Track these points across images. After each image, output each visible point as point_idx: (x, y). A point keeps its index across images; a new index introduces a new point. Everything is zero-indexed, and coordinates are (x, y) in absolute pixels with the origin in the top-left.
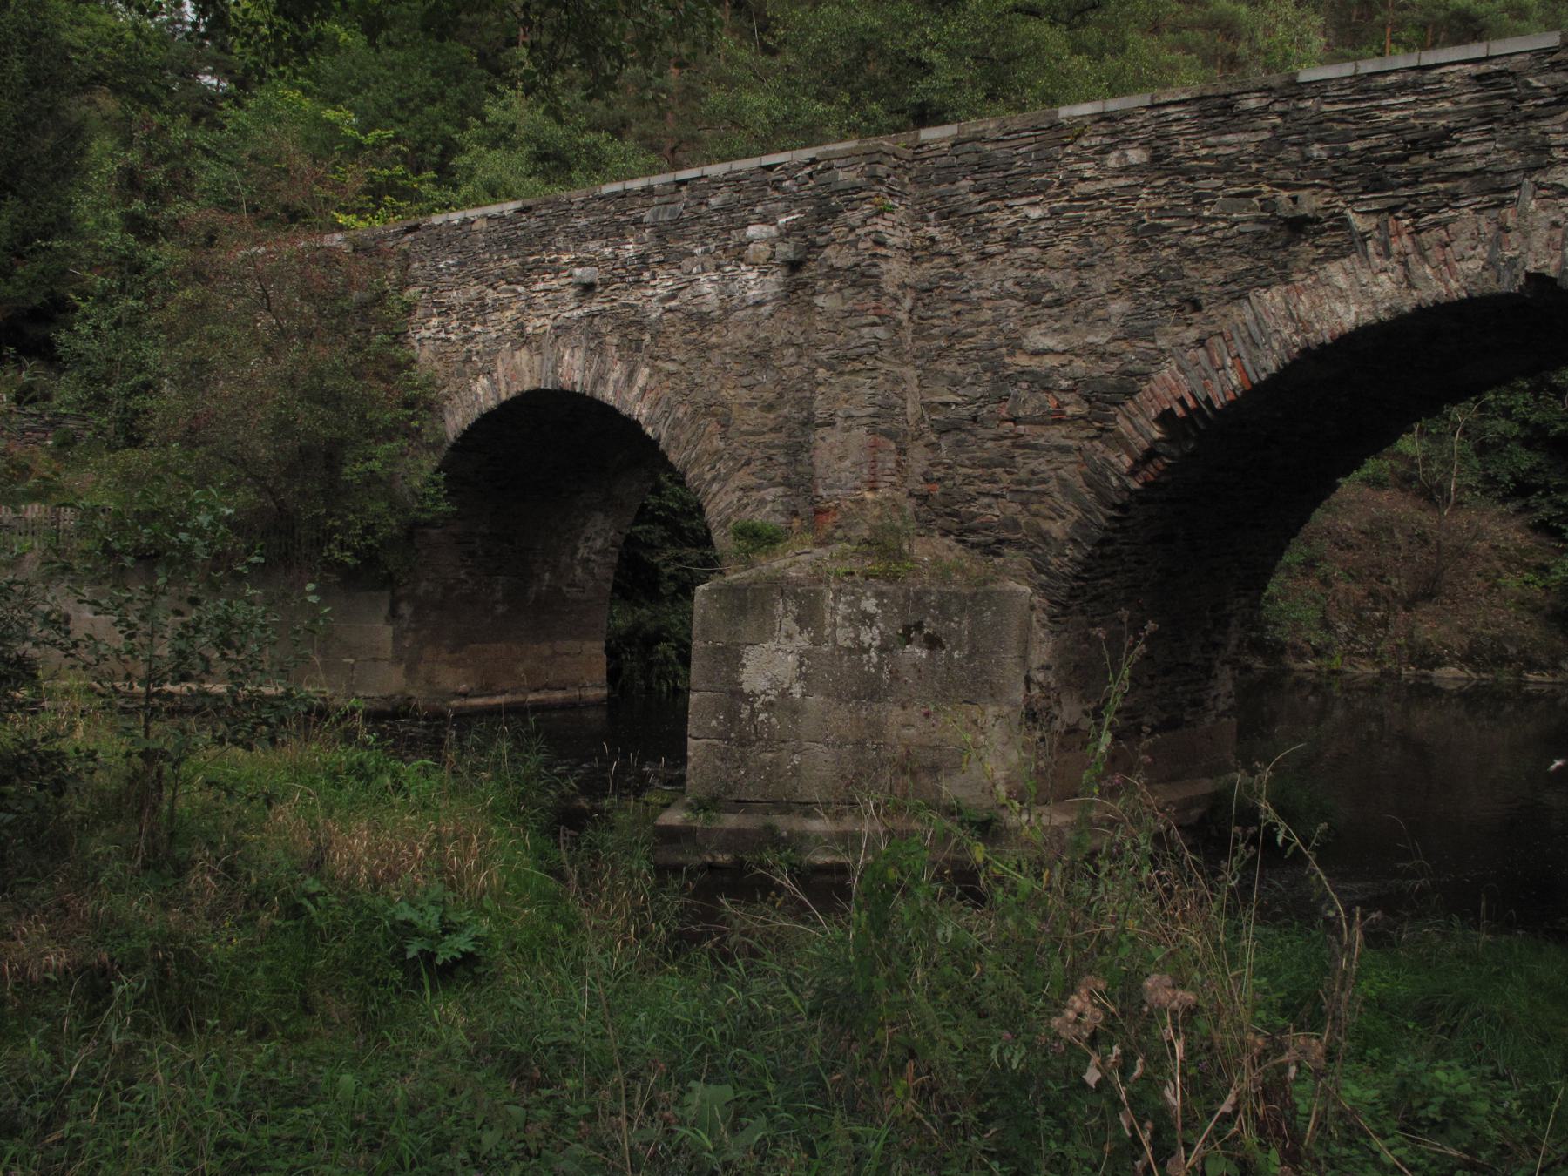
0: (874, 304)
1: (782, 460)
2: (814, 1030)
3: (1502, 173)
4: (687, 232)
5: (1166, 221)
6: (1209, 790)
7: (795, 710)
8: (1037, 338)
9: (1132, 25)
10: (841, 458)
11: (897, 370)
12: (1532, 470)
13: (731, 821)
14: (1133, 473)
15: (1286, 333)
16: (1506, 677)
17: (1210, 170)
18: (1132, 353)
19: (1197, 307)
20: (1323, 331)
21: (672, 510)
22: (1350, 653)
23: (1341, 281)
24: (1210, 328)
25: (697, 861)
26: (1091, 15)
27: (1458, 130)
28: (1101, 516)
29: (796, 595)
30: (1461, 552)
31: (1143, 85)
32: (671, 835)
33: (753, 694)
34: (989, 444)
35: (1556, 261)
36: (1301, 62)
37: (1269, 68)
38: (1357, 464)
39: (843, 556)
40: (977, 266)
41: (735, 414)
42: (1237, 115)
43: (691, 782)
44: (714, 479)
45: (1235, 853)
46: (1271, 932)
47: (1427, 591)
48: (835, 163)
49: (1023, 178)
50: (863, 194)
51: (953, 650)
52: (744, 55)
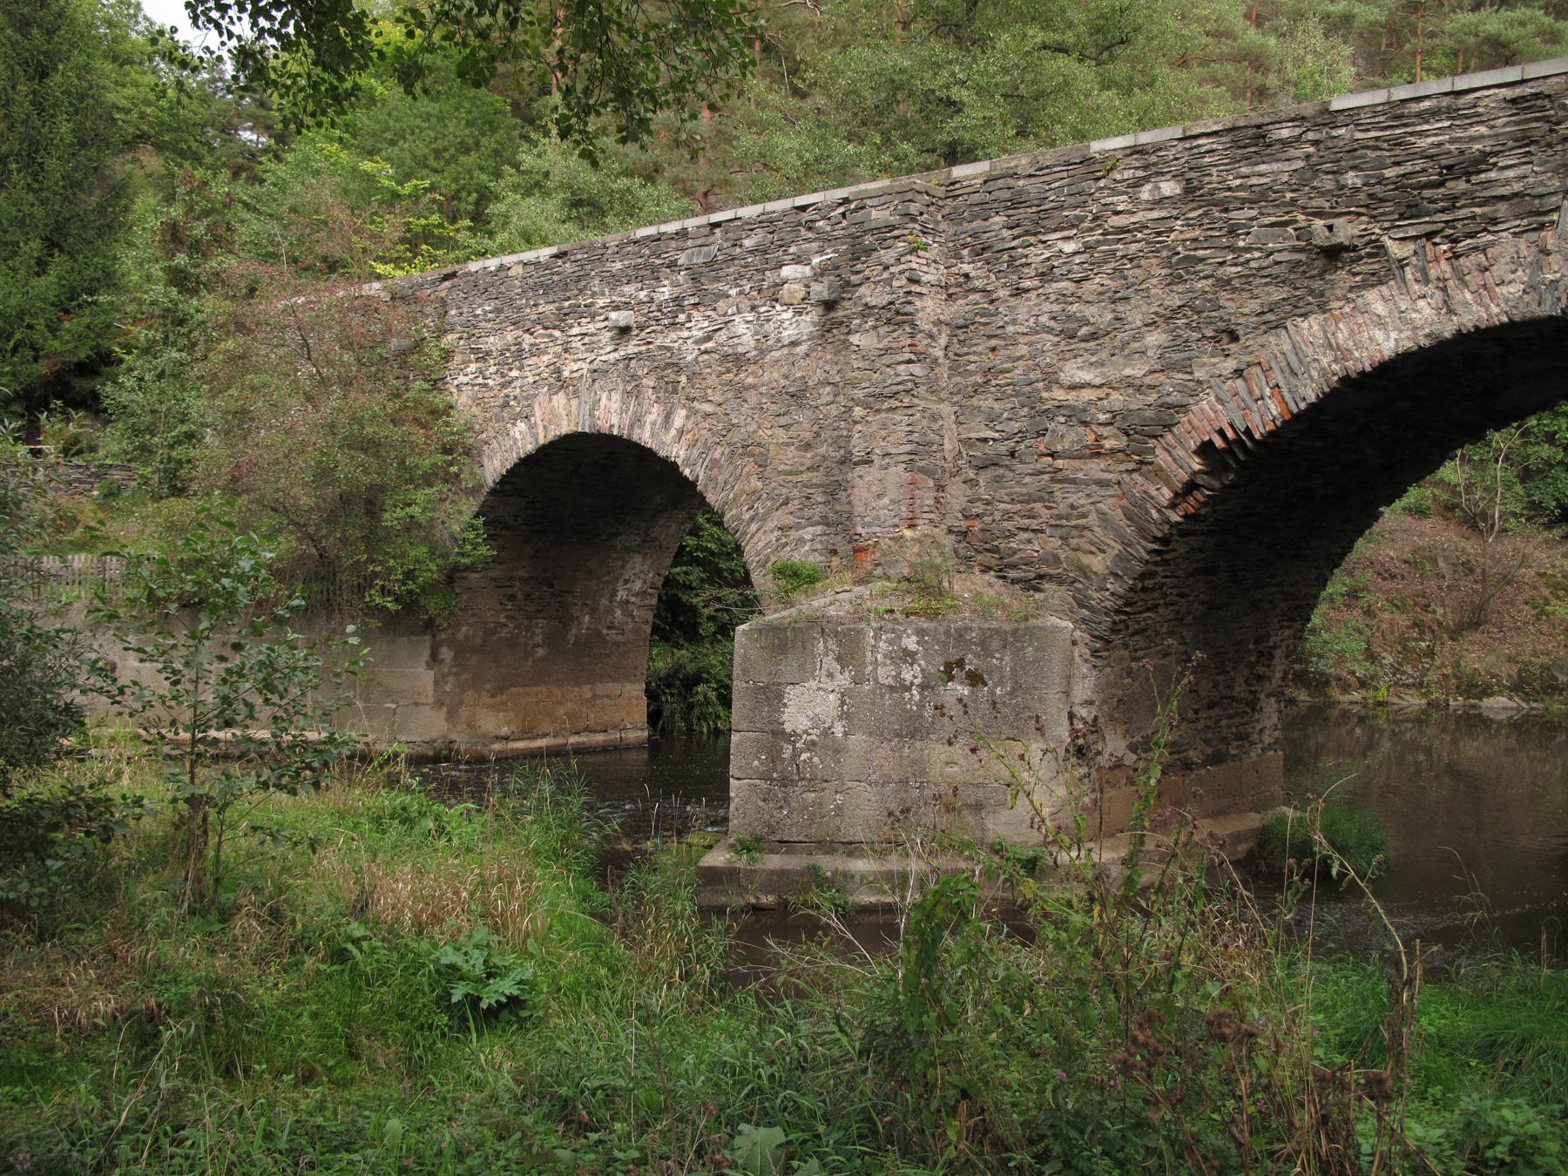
0: (909, 341)
2: (864, 1071)
3: (1541, 196)
4: (721, 273)
5: (1201, 253)
6: (1257, 824)
8: (1075, 372)
9: (1161, 60)
10: (879, 496)
13: (774, 862)
14: (1173, 506)
17: (1244, 201)
18: (1170, 385)
19: (1234, 338)
20: (1364, 359)
21: (712, 553)
23: (1380, 308)
25: (742, 903)
26: (1119, 50)
27: (1496, 154)
28: (1142, 549)
30: (1507, 580)
32: (713, 877)
34: (1028, 479)
36: (1331, 92)
38: (1400, 492)
39: (883, 595)
40: (1013, 302)
44: (752, 519)
47: (1473, 620)
48: (868, 202)
49: (1057, 213)
50: (896, 233)
51: (995, 686)
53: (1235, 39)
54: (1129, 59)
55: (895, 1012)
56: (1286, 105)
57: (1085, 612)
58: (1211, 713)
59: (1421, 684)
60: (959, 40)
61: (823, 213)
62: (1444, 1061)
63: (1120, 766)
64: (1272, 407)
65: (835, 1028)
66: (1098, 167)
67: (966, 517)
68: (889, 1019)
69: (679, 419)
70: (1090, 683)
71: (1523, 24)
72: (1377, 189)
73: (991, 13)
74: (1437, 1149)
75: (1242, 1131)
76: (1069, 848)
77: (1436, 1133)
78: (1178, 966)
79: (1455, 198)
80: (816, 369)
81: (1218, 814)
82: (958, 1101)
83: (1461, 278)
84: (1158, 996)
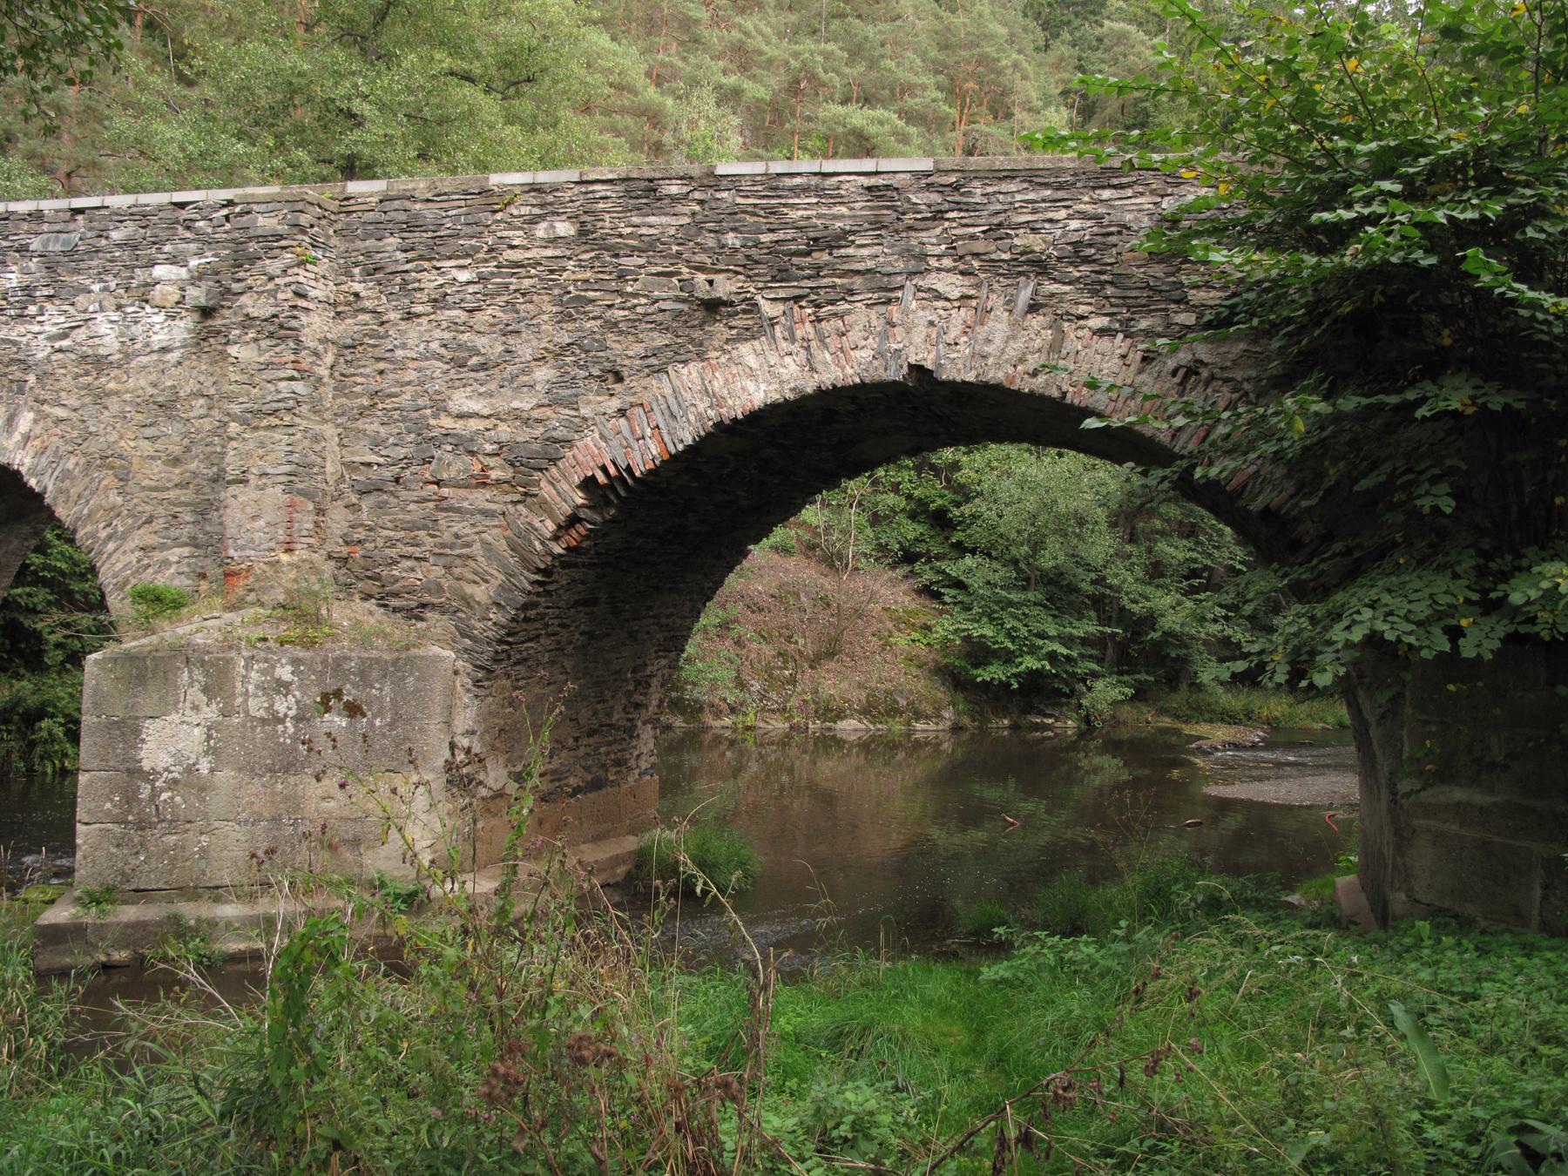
0: (293, 357)
1: (188, 519)
2: (226, 1135)
3: (889, 275)
4: (82, 265)
5: (591, 294)
6: (635, 847)
7: (203, 788)
8: (462, 400)
9: (566, 103)
10: (255, 518)
11: (317, 428)
12: (916, 540)
13: (130, 913)
14: (556, 538)
15: (701, 407)
16: (897, 726)
17: (634, 249)
18: (557, 420)
19: (619, 378)
20: (736, 407)
21: (62, 573)
22: (763, 709)
23: (752, 361)
24: (631, 399)
25: (89, 961)
26: (525, 88)
27: (853, 233)
28: (525, 580)
29: (203, 663)
30: (858, 614)
31: (573, 161)
32: (55, 935)
33: (154, 771)
34: (412, 507)
35: (932, 356)
36: (720, 157)
37: (691, 159)
38: (766, 532)
39: (256, 622)
40: (403, 325)
41: (135, 467)
42: (660, 199)
43: (80, 873)
44: (110, 537)
45: (656, 907)
46: (695, 980)
47: (829, 651)
48: (255, 207)
49: (452, 241)
50: (284, 243)
51: (375, 717)
52: (156, 81)
53: (636, 94)
54: (538, 100)
55: (261, 1066)
56: (679, 164)
57: (468, 641)
58: (591, 741)
59: (784, 710)
60: (364, 52)
61: (205, 213)
62: (799, 1056)
63: (501, 796)
64: (652, 447)
65: (192, 1091)
66: (496, 200)
67: (347, 543)
68: (253, 1075)
69: (25, 421)
70: (471, 713)
71: (881, 123)
72: (753, 251)
73: (399, 30)
74: (791, 1137)
75: (601, 1150)
76: (443, 881)
77: (791, 1122)
78: (551, 993)
79: (820, 268)
80: (190, 378)
81: (598, 838)
82: (330, 1154)
83: (822, 339)
84: (534, 1023)
